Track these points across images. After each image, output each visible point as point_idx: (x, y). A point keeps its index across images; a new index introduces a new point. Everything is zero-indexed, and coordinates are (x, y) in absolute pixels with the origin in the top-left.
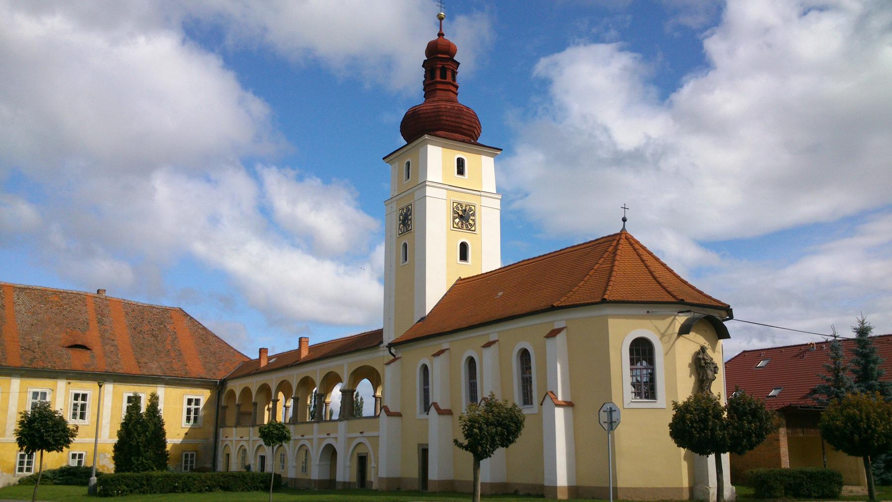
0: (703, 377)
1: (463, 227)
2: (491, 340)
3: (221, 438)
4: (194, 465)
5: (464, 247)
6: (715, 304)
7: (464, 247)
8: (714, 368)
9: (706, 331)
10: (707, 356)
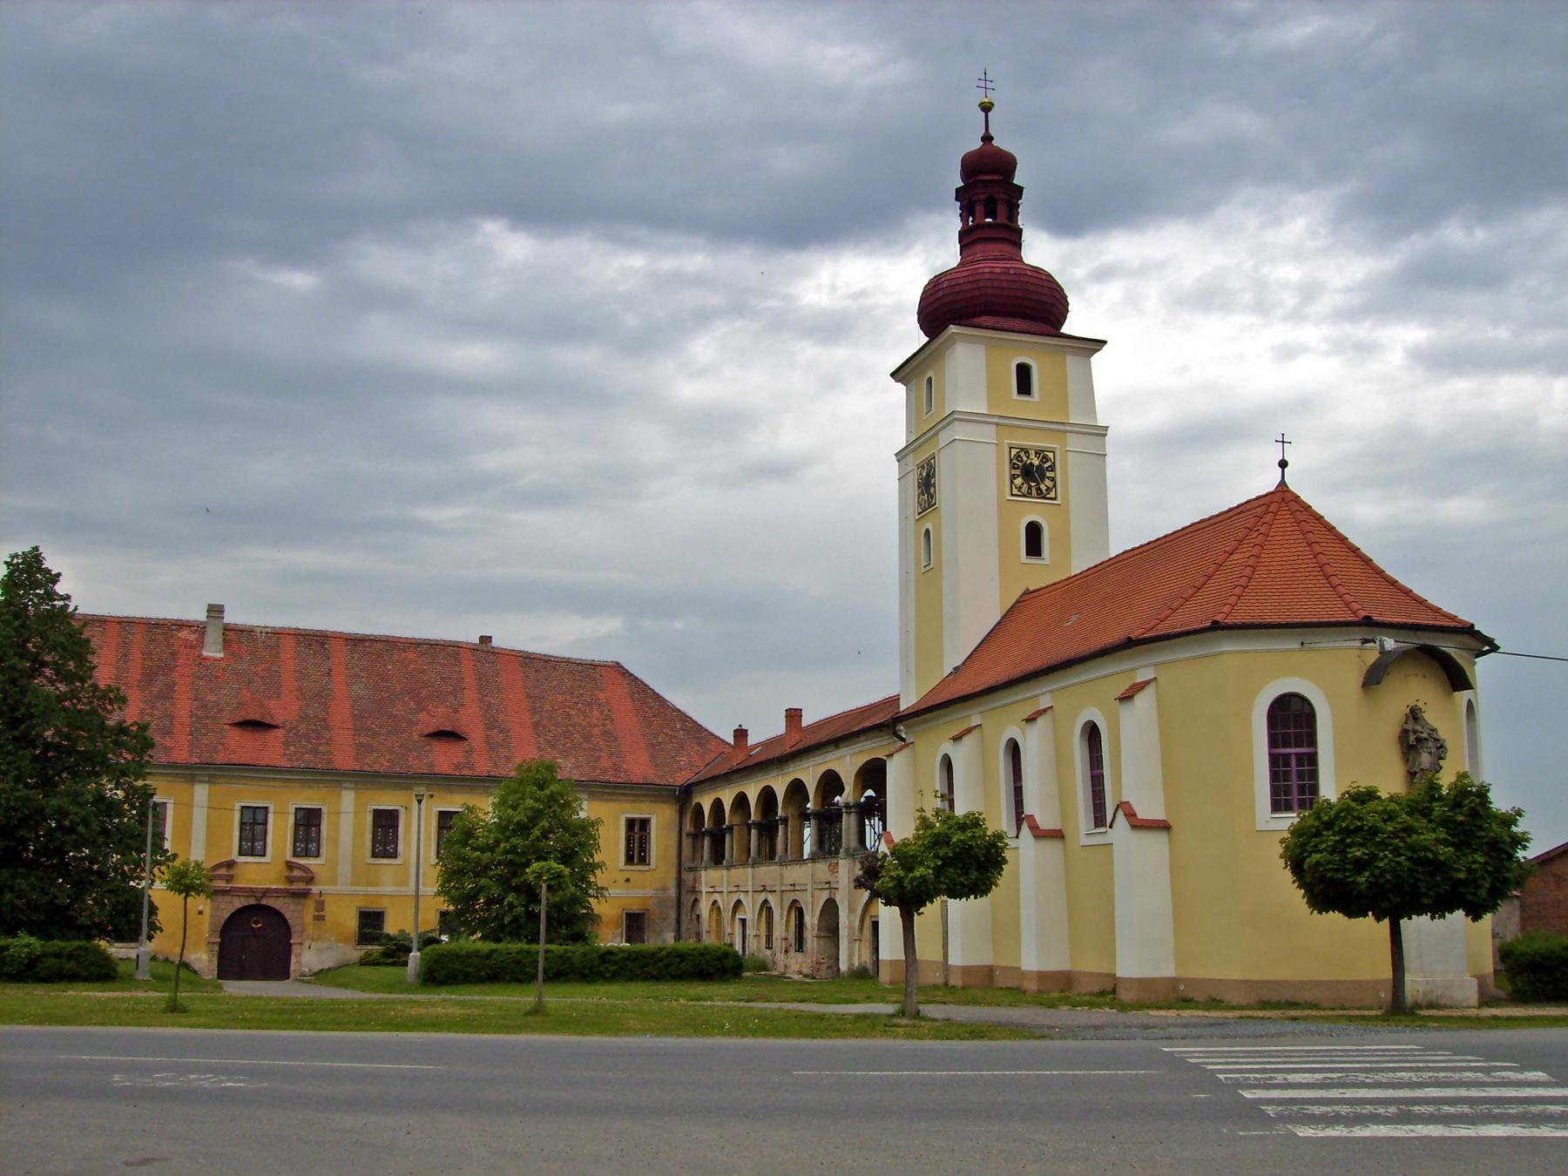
1: (1031, 494)
2: (1042, 708)
5: (1034, 531)
6: (1453, 624)
7: (1034, 531)
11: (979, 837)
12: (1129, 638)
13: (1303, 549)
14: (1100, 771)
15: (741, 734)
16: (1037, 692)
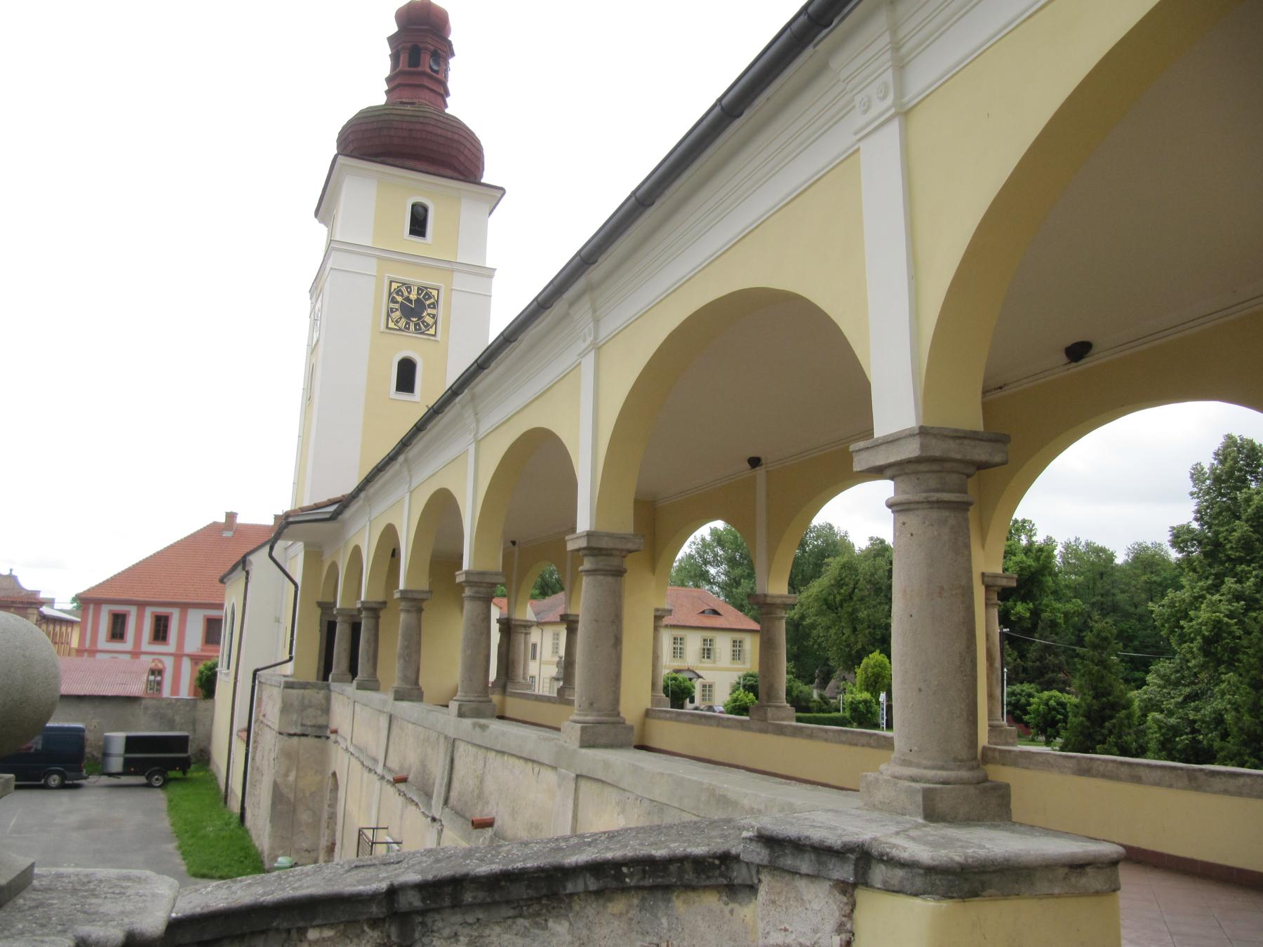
1: (408, 329)
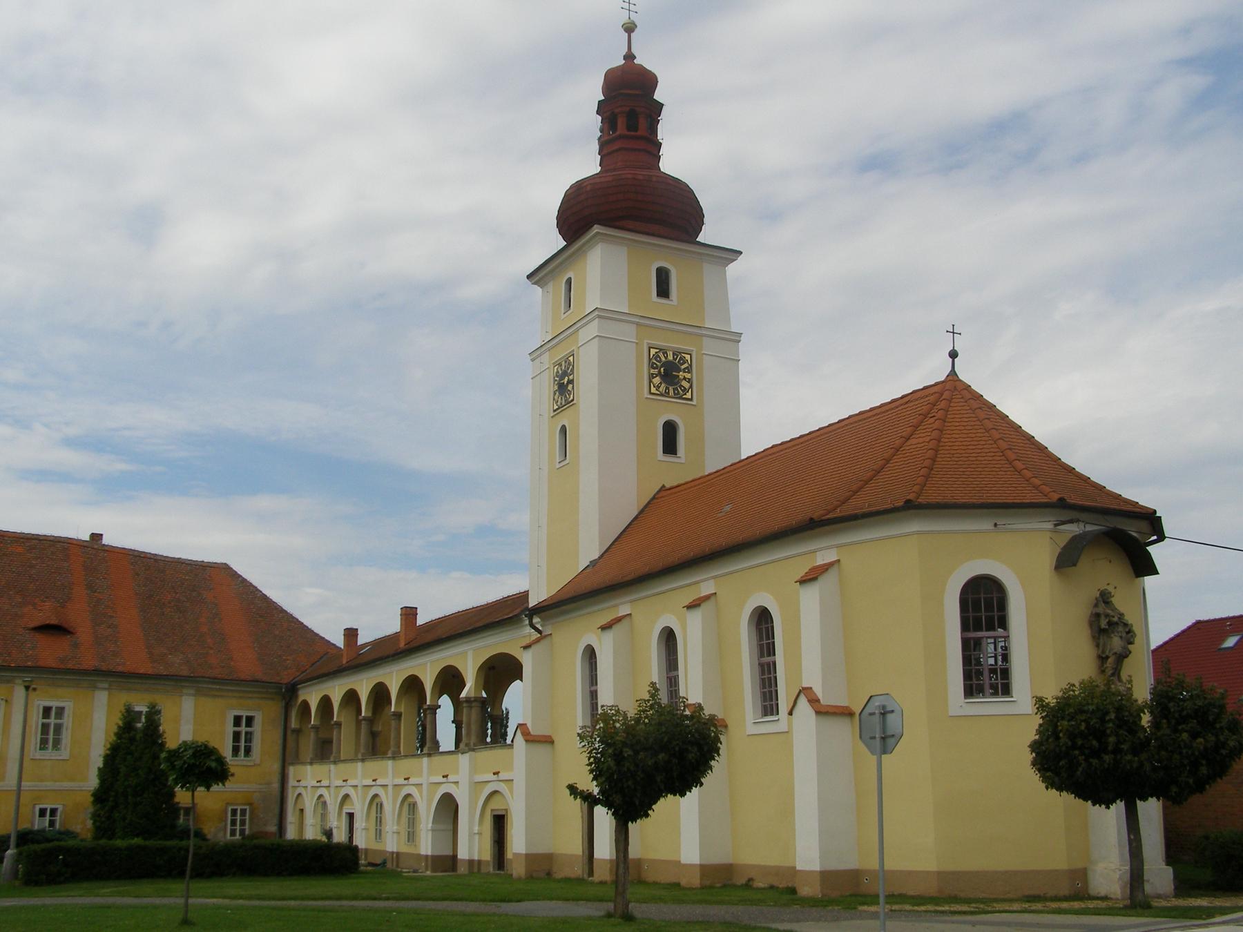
0: (1103, 652)
2: (620, 615)
3: (292, 782)
4: (247, 827)
5: (670, 431)
6: (1129, 508)
7: (670, 431)
8: (1128, 632)
9: (1110, 562)
10: (1114, 609)
11: (1198, 696)
12: (811, 519)
13: (982, 435)
14: (676, 672)
15: (351, 634)
16: (698, 579)
